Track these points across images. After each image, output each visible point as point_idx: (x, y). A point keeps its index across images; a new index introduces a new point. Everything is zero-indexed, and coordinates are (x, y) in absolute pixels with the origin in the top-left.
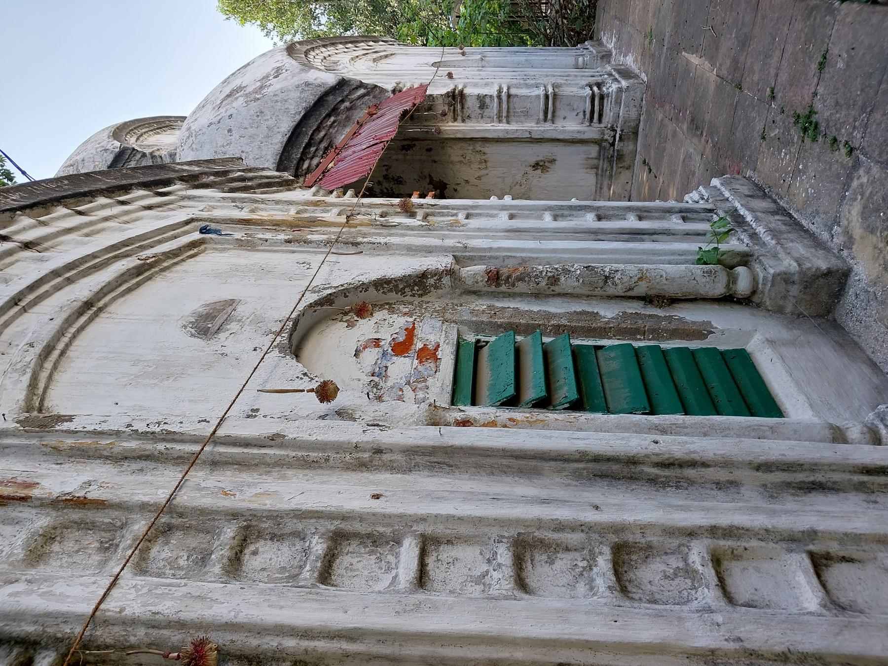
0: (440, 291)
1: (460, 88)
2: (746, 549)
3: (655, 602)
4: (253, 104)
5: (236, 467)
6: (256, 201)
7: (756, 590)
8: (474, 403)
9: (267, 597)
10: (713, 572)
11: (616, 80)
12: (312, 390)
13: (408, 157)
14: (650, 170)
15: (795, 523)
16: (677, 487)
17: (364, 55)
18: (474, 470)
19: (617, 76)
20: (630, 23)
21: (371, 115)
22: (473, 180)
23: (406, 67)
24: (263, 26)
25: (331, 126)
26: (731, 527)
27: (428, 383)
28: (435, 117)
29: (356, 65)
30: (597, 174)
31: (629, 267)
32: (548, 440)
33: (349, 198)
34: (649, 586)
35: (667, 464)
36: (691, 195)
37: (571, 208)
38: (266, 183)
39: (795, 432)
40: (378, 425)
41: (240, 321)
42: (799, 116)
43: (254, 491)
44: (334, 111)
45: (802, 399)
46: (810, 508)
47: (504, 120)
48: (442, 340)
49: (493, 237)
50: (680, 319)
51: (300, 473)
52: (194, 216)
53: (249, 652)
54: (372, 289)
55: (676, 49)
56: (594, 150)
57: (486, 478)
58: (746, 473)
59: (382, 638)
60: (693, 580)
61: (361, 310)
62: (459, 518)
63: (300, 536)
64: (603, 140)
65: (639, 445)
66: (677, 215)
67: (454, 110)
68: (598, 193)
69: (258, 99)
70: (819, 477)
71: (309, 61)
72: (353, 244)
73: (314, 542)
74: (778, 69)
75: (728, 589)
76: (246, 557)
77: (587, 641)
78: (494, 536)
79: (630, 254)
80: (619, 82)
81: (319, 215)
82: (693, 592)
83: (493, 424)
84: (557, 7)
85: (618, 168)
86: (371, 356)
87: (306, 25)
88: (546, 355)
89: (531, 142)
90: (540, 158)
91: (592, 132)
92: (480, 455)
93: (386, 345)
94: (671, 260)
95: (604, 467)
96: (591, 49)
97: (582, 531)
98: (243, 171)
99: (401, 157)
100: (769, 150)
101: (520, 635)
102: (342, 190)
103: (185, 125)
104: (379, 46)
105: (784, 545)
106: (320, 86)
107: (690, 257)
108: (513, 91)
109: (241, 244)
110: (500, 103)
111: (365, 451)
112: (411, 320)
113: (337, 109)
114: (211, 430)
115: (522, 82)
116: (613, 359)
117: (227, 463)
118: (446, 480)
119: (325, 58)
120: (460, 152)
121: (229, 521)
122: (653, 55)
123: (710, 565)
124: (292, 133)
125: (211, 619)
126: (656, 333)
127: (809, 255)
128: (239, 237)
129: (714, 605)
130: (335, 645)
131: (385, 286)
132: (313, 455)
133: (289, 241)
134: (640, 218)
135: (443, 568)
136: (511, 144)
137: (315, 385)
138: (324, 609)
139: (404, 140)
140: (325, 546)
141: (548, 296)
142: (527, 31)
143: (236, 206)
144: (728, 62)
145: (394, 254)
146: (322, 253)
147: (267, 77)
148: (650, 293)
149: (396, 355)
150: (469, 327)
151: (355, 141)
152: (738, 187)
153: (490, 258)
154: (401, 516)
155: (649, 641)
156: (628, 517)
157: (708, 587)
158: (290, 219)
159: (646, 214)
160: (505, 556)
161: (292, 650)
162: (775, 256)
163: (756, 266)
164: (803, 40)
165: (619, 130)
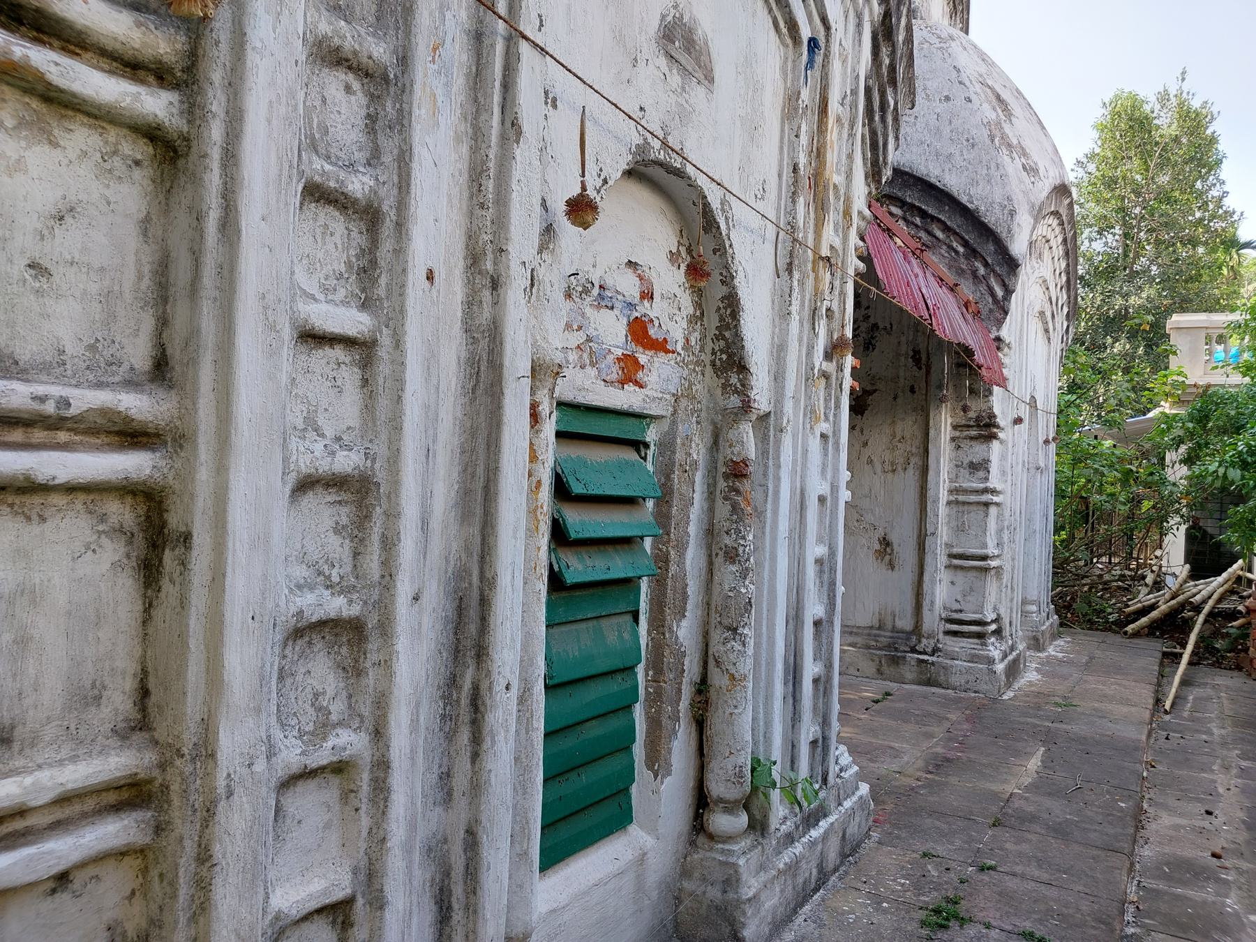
0: (719, 391)
1: (1001, 435)
2: (357, 810)
3: (281, 678)
4: (986, 133)
5: (474, 69)
6: (852, 126)
7: (299, 822)
8: (560, 435)
9: (284, 100)
10: (325, 762)
11: (1005, 656)
12: (584, 188)
13: (903, 359)
14: (877, 702)
15: (394, 880)
16: (443, 717)
17: (1050, 298)
18: (469, 425)
19: (1010, 658)
20: (1085, 678)
21: (966, 306)
22: (867, 452)
23: (1031, 358)
24: (1091, 157)
25: (950, 247)
26: (389, 790)
27: (588, 368)
28: (960, 397)
29: (1036, 286)
30: (871, 627)
31: (750, 662)
32: (511, 533)
33: (854, 264)
34: (303, 670)
35: (477, 703)
36: (846, 754)
37: (832, 584)
38: (877, 142)
39: (521, 887)
40: (532, 285)
41: (683, 89)
42: (956, 903)
43: (439, 92)
44: (973, 253)
45: (563, 899)
46: (415, 902)
47: (952, 498)
48: (649, 393)
49: (794, 471)
50: (675, 732)
51: (463, 166)
52: (833, 31)
53: (201, 69)
54: (723, 291)
55: (1049, 738)
56: (906, 623)
57: (456, 441)
58: (463, 815)
59: (225, 273)
60: (312, 734)
61: (695, 269)
62: (400, 397)
63: (374, 159)
64: (920, 636)
65: (504, 663)
66: (819, 733)
67: (969, 426)
68: (847, 630)
69: (993, 141)
70: (457, 916)
71: (1044, 218)
72: (790, 264)
73: (365, 179)
74: (1023, 877)
75: (300, 783)
76: (343, 76)
77: (224, 575)
78: (375, 448)
79: (768, 664)
80: (1002, 660)
81: (833, 217)
82: (295, 733)
83: (533, 458)
84: (1107, 577)
85: (880, 657)
86: (628, 285)
87: (1091, 220)
88: (625, 542)
89: (919, 536)
90: (895, 547)
91: (932, 621)
92: (490, 434)
93: (644, 308)
94: (757, 723)
95: (473, 613)
96: (1047, 624)
97: (383, 576)
98: (896, 109)
99: (904, 348)
100: (908, 862)
101: (231, 477)
102: (865, 254)
103: (956, 32)
104: (1061, 322)
105: (363, 863)
106: (1009, 231)
107: (761, 749)
108: (993, 510)
109: (792, 98)
110: (977, 492)
111: (495, 264)
112: (679, 349)
113: (975, 257)
114: (528, 33)
115: (1006, 524)
116: (620, 636)
117: (479, 55)
118: (453, 383)
119: (1048, 241)
120: (908, 435)
121: (395, 52)
122: (1039, 708)
123: (335, 759)
124: (941, 191)
125: (249, 9)
126: (655, 698)
127: (763, 913)
128: (802, 95)
129: (279, 761)
130: (214, 200)
131: (729, 311)
132: (490, 185)
133: (795, 169)
134: (816, 681)
135: (328, 370)
136: (918, 506)
137: (591, 193)
138: (268, 185)
139: (928, 354)
140: (359, 195)
141: (709, 547)
142: (1072, 537)
143: (845, 96)
144: (1031, 809)
145: (774, 326)
146: (778, 218)
147: (1024, 154)
148: (712, 690)
149: (629, 324)
150: (667, 433)
151: (931, 279)
152: (857, 819)
153: (766, 466)
154: (402, 311)
155: (226, 664)
156: (402, 643)
157: (303, 753)
158: (827, 173)
159: (822, 689)
160: (346, 462)
161: (205, 134)
162: (762, 868)
163: (748, 841)
164: (1065, 911)
165: (934, 659)
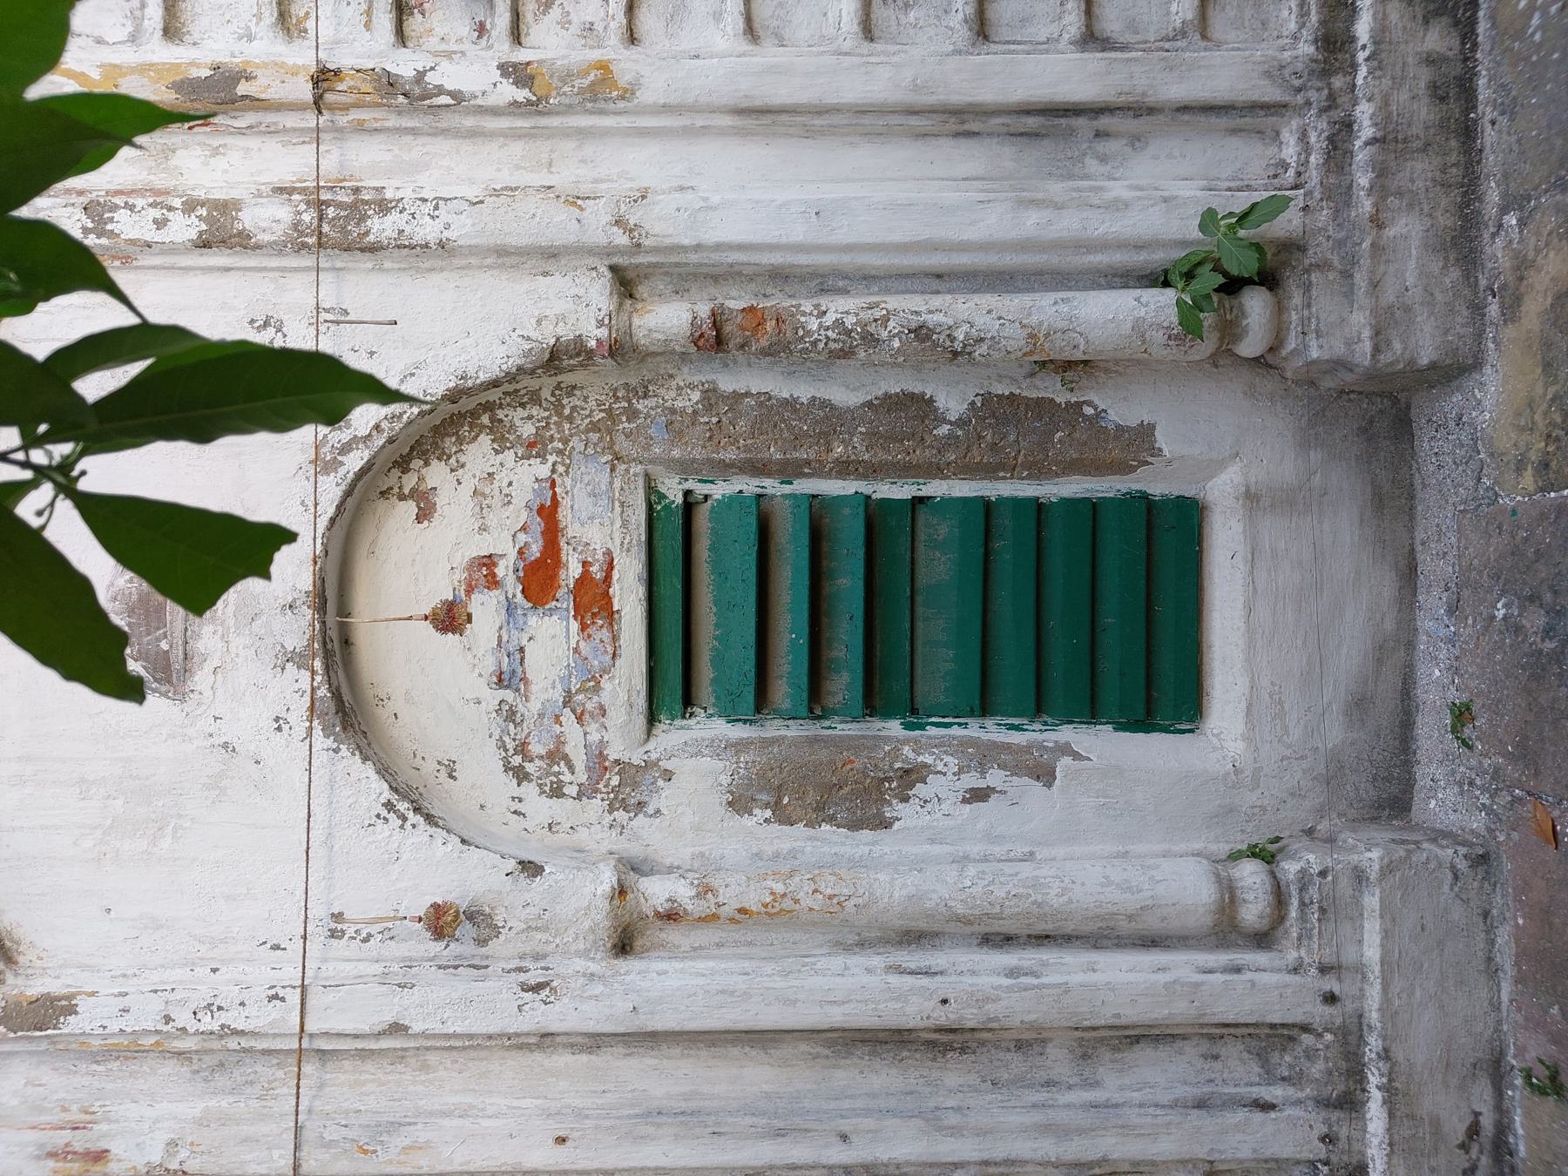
57: (704, 1053)
112: (544, 471)
145: (469, 267)
